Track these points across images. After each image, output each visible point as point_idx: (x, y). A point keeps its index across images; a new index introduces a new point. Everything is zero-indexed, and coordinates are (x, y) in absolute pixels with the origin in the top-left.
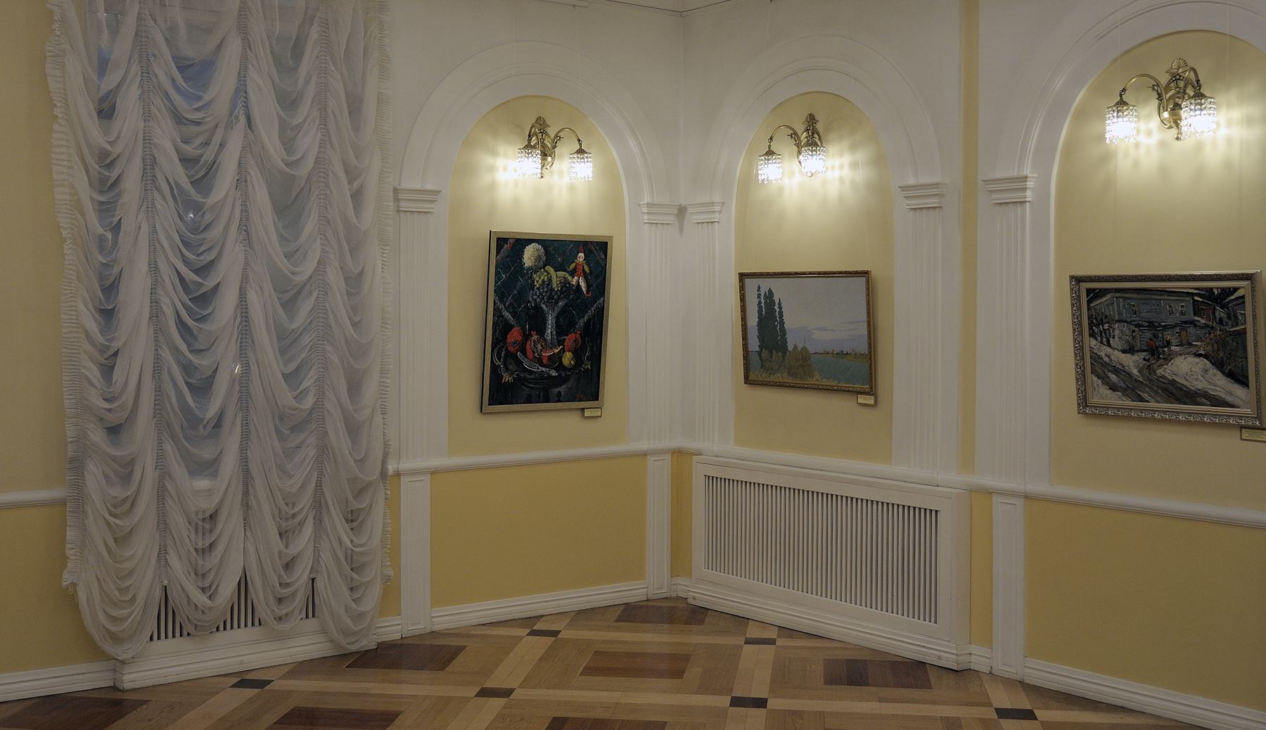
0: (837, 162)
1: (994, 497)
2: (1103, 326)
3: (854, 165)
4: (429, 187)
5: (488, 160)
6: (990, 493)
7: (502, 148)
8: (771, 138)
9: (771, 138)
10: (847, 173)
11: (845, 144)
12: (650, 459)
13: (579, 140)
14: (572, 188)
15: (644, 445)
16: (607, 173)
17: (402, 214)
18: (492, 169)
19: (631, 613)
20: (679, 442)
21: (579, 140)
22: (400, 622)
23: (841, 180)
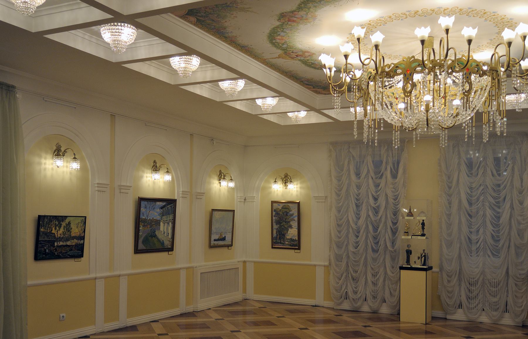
0: (295, 186)
1: (317, 267)
2: (154, 224)
3: (301, 188)
4: (128, 185)
5: (36, 159)
6: (316, 266)
7: (146, 171)
8: (276, 179)
9: (276, 179)
10: (299, 189)
11: (299, 182)
12: (121, 278)
13: (74, 154)
14: (71, 173)
15: (179, 266)
16: (83, 168)
17: (121, 193)
18: (40, 164)
19: (182, 315)
20: (244, 259)
21: (74, 154)
22: (105, 328)
23: (297, 191)
